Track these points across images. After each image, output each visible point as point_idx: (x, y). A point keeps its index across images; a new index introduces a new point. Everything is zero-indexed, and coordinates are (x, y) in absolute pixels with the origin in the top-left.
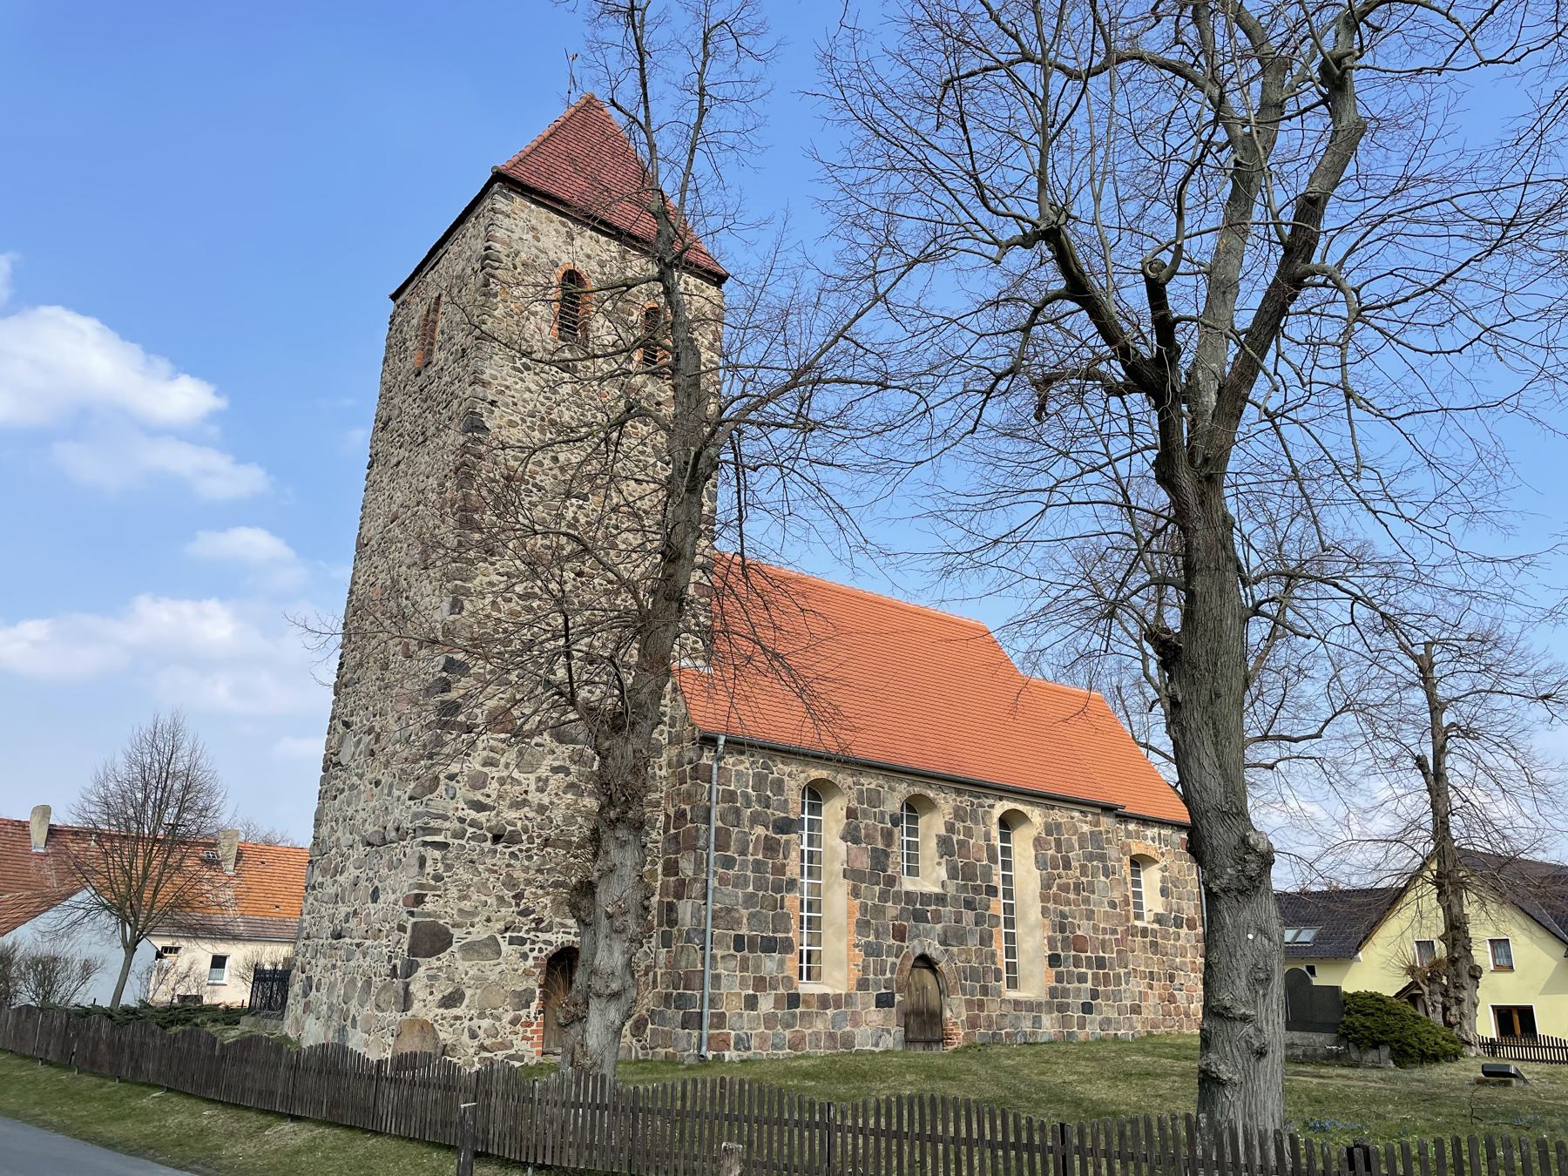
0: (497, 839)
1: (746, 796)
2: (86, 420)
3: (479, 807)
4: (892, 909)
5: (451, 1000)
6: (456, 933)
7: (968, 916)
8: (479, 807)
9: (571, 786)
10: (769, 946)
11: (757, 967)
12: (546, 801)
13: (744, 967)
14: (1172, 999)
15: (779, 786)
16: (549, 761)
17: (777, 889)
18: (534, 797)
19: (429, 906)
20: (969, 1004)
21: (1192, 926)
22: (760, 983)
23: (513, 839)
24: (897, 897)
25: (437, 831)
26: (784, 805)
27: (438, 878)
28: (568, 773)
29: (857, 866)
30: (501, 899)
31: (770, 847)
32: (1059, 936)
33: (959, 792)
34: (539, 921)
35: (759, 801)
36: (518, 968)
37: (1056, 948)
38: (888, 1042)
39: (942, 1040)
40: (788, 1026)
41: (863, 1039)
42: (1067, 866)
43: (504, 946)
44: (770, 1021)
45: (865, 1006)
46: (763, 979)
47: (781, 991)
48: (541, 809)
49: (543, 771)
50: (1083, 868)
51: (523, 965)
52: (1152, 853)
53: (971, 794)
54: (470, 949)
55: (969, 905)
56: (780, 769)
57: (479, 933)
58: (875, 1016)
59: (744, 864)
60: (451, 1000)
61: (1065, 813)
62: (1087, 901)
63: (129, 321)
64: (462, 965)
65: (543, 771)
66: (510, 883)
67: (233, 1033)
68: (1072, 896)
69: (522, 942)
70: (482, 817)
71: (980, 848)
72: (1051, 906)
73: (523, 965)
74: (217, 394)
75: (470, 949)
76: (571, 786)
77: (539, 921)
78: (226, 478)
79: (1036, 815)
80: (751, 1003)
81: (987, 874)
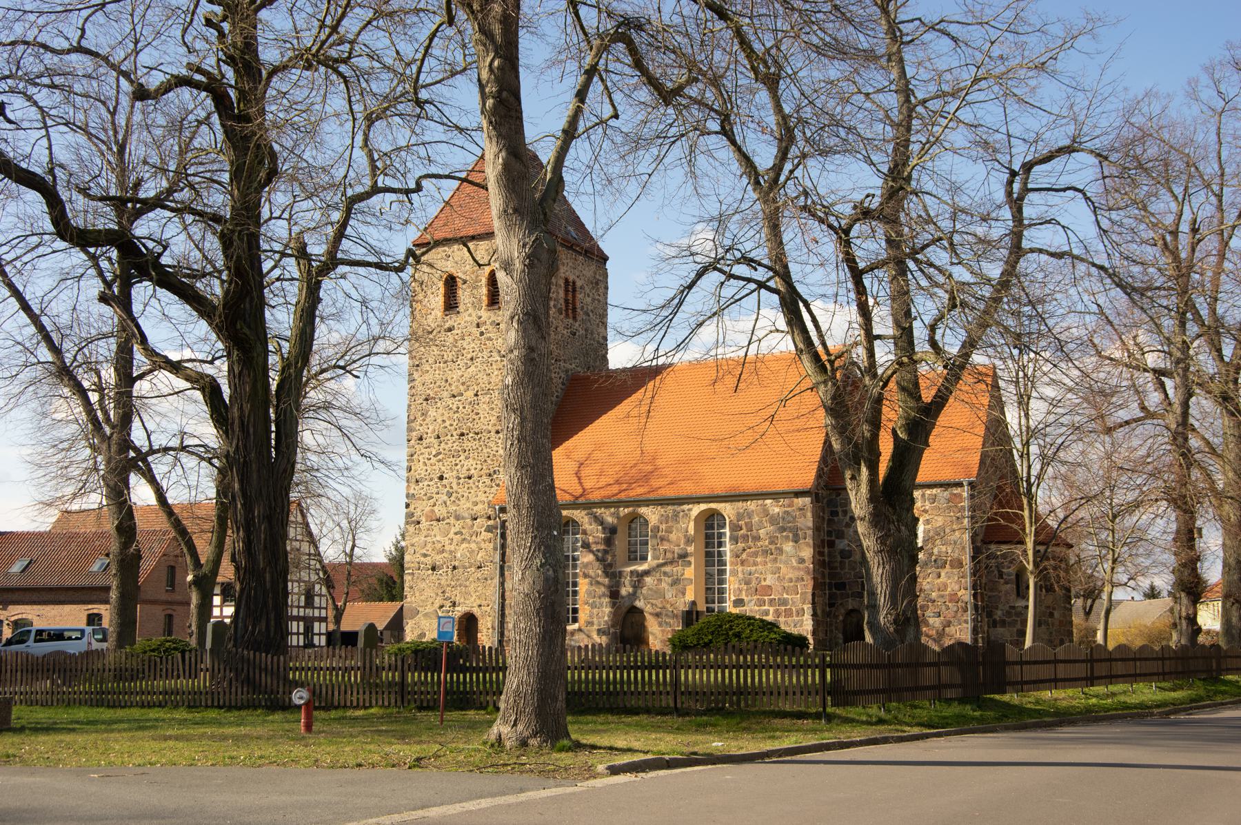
3: (425, 556)
8: (425, 556)
16: (453, 530)
28: (462, 534)
64: (424, 622)
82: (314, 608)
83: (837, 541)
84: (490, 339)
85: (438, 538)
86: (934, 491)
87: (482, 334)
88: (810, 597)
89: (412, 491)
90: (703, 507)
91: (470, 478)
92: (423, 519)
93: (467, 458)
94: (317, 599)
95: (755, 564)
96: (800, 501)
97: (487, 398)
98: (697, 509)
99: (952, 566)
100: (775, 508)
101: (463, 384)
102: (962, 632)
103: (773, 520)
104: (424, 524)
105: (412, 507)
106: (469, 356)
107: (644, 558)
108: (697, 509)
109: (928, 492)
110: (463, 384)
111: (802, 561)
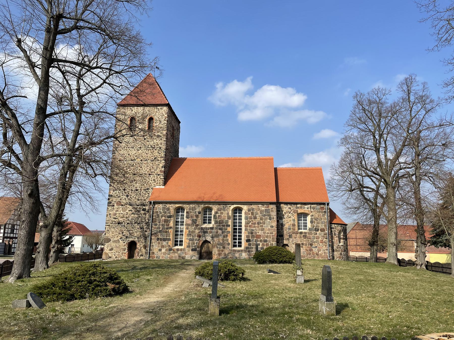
0: (119, 224)
1: (160, 212)
2: (278, 111)
3: (115, 218)
4: (197, 231)
5: (111, 249)
6: (112, 239)
7: (220, 232)
8: (115, 218)
9: (133, 213)
10: (164, 240)
11: (162, 244)
12: (128, 216)
13: (159, 243)
14: (311, 250)
15: (168, 209)
16: (128, 209)
17: (167, 229)
18: (125, 216)
19: (107, 235)
20: (219, 251)
21: (322, 230)
22: (163, 246)
23: (121, 223)
24: (199, 229)
25: (108, 223)
26: (170, 213)
27: (108, 231)
28: (132, 211)
29: (188, 223)
30: (119, 233)
31: (166, 221)
32: (250, 235)
33: (219, 204)
34: (127, 237)
35: (163, 212)
36: (124, 245)
37: (249, 237)
38: (194, 258)
39: (211, 258)
40: (168, 254)
41: (188, 257)
42: (255, 218)
43: (120, 241)
44: (164, 253)
45: (189, 251)
46: (163, 246)
47: (167, 248)
48: (127, 218)
49: (127, 211)
50: (261, 219)
51: (124, 244)
52: (307, 212)
53: (223, 205)
54: (115, 241)
55: (220, 229)
56: (168, 206)
57: (116, 239)
58: (191, 253)
59: (160, 225)
60: (111, 249)
61: (256, 206)
62: (262, 226)
63: (283, 83)
64: (112, 244)
65: (127, 211)
66: (121, 231)
67: (362, 277)
68: (256, 225)
69: (124, 240)
70: (115, 220)
71: (225, 216)
72: (248, 228)
73: (124, 244)
74: (304, 95)
75: (115, 241)
76: (133, 213)
77: (127, 237)
78: (314, 117)
79: (245, 208)
80: (160, 250)
81: (227, 222)
82: (14, 234)
83: (280, 220)
84: (148, 141)
85: (122, 212)
86: (314, 206)
87: (145, 139)
88: (276, 240)
89: (111, 194)
90: (235, 206)
91: (137, 190)
92: (115, 204)
93: (136, 183)
94: (15, 230)
95: (255, 227)
96: (271, 206)
97: (146, 162)
98: (233, 207)
99: (321, 231)
100: (263, 208)
101: (136, 156)
102: (369, 253)
103: (261, 212)
104: (116, 206)
105: (111, 199)
106: (139, 147)
107: (210, 223)
108: (233, 207)
109: (312, 206)
110: (136, 156)
111: (272, 227)
